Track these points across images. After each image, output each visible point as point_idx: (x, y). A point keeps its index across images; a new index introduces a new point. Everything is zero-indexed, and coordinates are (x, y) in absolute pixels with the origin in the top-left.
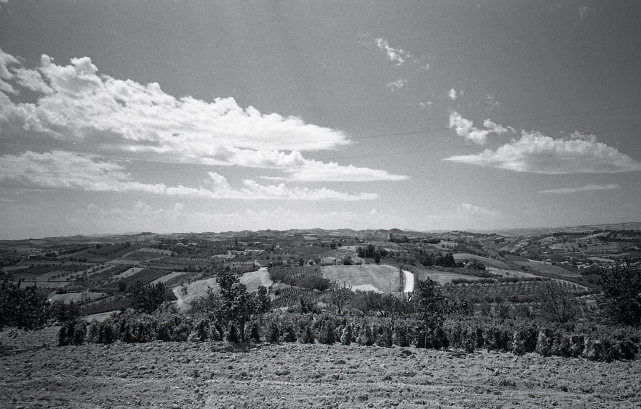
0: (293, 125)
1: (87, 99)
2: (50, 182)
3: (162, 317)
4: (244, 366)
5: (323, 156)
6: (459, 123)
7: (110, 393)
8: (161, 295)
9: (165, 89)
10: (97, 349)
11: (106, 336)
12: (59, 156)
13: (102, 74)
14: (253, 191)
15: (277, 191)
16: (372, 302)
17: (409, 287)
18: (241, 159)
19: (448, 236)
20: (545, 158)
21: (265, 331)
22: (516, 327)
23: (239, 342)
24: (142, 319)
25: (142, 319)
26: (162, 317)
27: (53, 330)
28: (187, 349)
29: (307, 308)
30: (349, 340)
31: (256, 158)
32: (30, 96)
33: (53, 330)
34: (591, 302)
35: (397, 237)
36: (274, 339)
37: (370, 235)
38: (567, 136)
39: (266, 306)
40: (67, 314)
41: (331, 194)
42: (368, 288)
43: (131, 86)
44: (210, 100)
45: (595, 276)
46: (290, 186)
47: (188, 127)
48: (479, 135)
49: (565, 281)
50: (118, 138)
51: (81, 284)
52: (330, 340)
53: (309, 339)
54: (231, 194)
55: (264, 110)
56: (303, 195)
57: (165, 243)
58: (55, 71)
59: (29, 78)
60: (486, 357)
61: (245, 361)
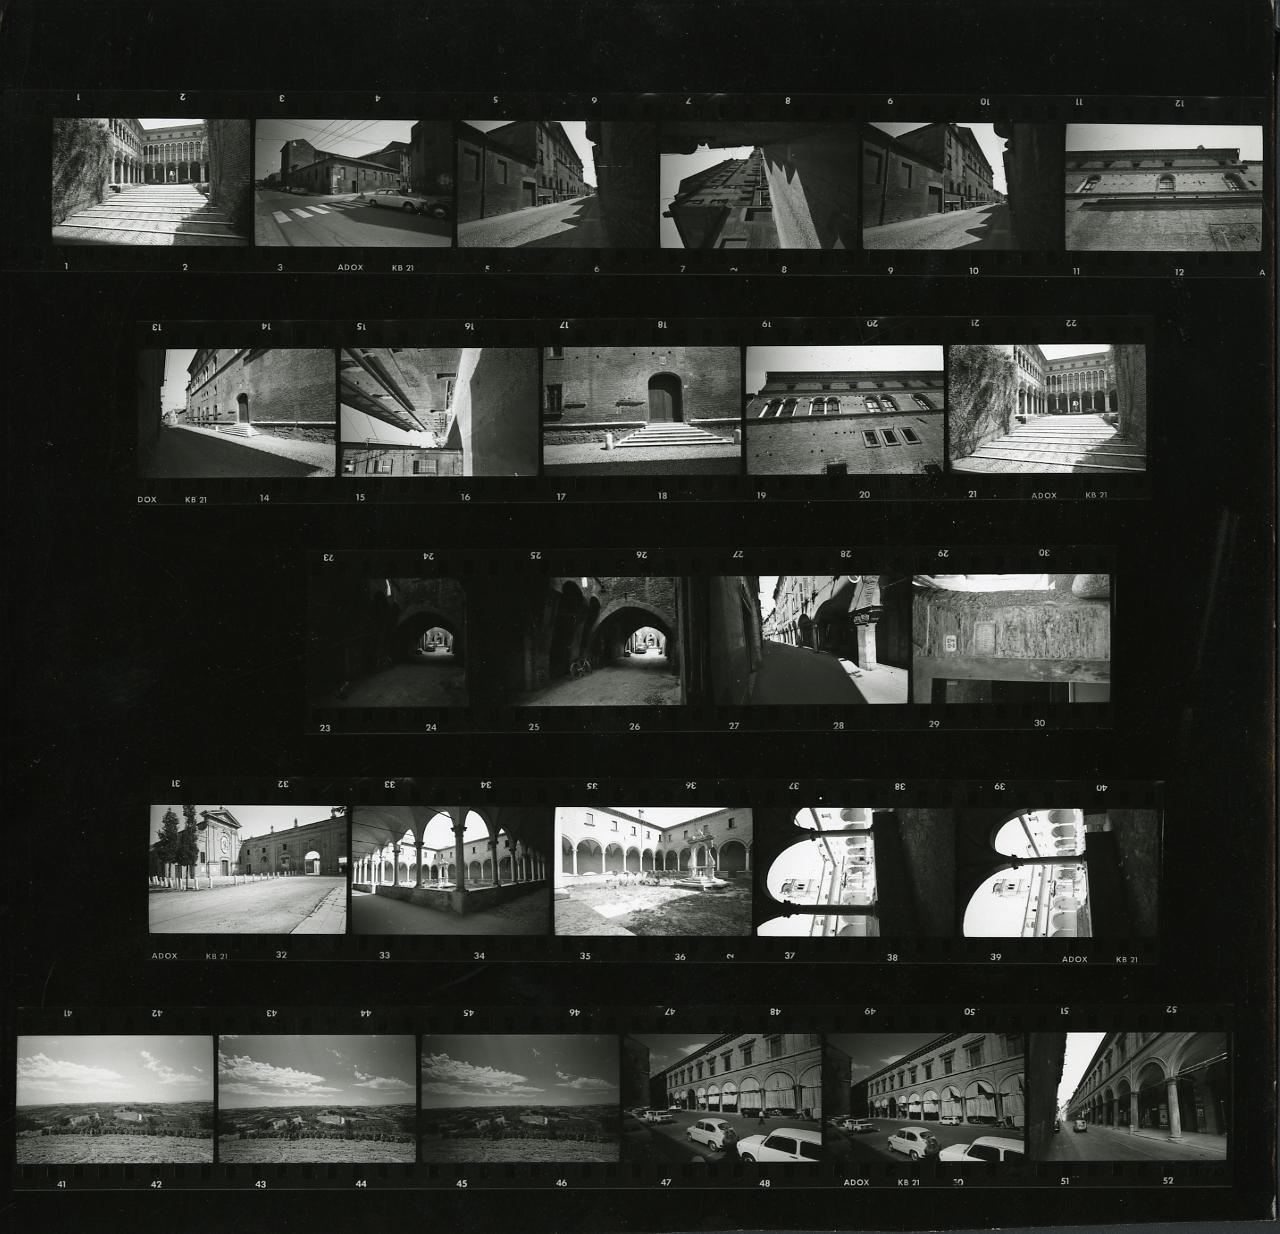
0: (308, 1075)
1: (248, 1068)
2: (237, 1092)
3: (270, 1131)
4: (293, 1145)
5: (318, 1084)
6: (358, 1075)
7: (254, 1153)
8: (270, 1125)
9: (271, 1065)
10: (453, 1140)
11: (253, 1136)
12: (239, 1085)
13: (432, 1054)
14: (297, 1094)
15: (304, 1094)
16: (332, 1126)
17: (343, 1122)
18: (293, 1085)
19: (558, 1107)
20: (383, 1085)
21: (102, 1131)
22: (374, 1134)
23: (293, 1139)
24: (63, 1128)
25: (63, 1128)
26: (270, 1131)
27: (238, 1135)
28: (277, 1140)
29: (313, 1128)
30: (325, 1137)
31: (298, 1085)
32: (231, 1067)
33: (238, 1135)
34: (600, 1126)
35: (339, 1108)
36: (303, 1137)
37: (331, 1107)
38: (390, 1078)
39: (301, 1128)
40: (242, 1131)
41: (319, 1095)
42: (130, 1119)
43: (459, 1063)
44: (284, 1068)
45: (399, 1119)
46: (511, 1093)
47: (478, 1075)
48: (364, 1078)
49: (390, 1120)
50: (256, 1079)
51: (246, 1122)
52: (319, 1137)
53: (313, 1137)
54: (491, 1095)
55: (300, 1071)
56: (513, 1095)
57: (271, 1109)
58: (238, 1060)
59: (231, 1062)
60: (366, 1142)
61: (295, 1143)
